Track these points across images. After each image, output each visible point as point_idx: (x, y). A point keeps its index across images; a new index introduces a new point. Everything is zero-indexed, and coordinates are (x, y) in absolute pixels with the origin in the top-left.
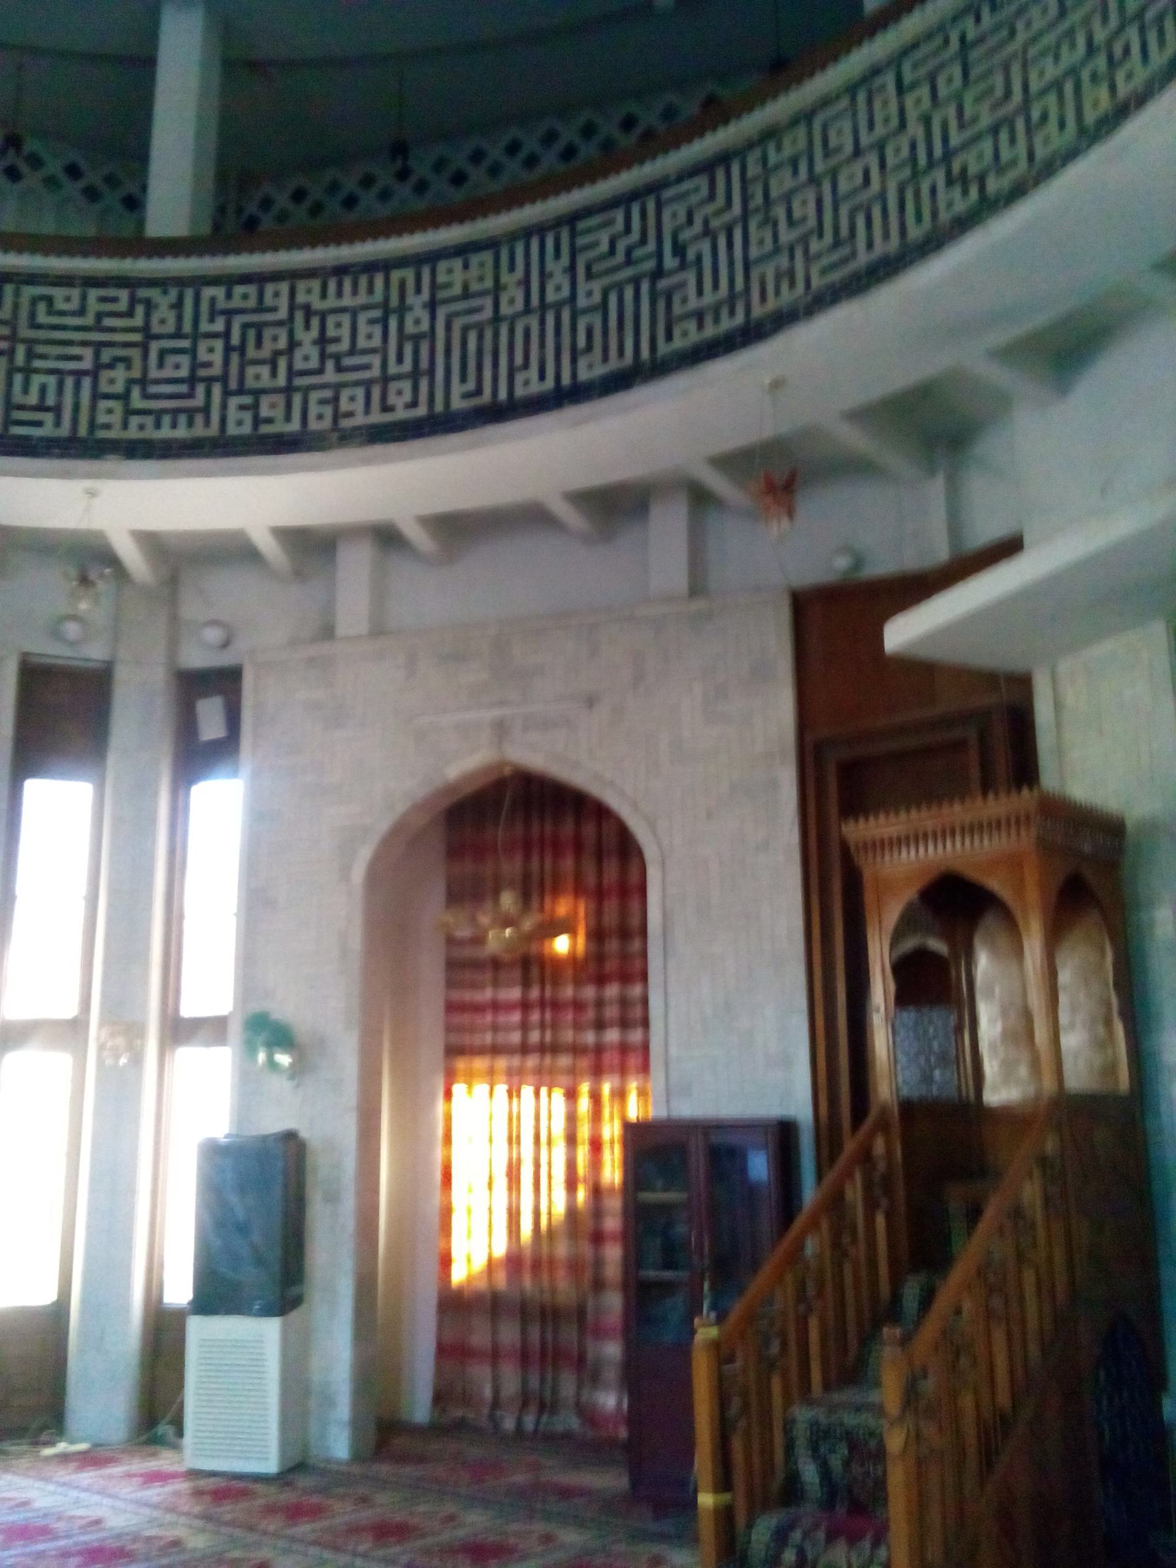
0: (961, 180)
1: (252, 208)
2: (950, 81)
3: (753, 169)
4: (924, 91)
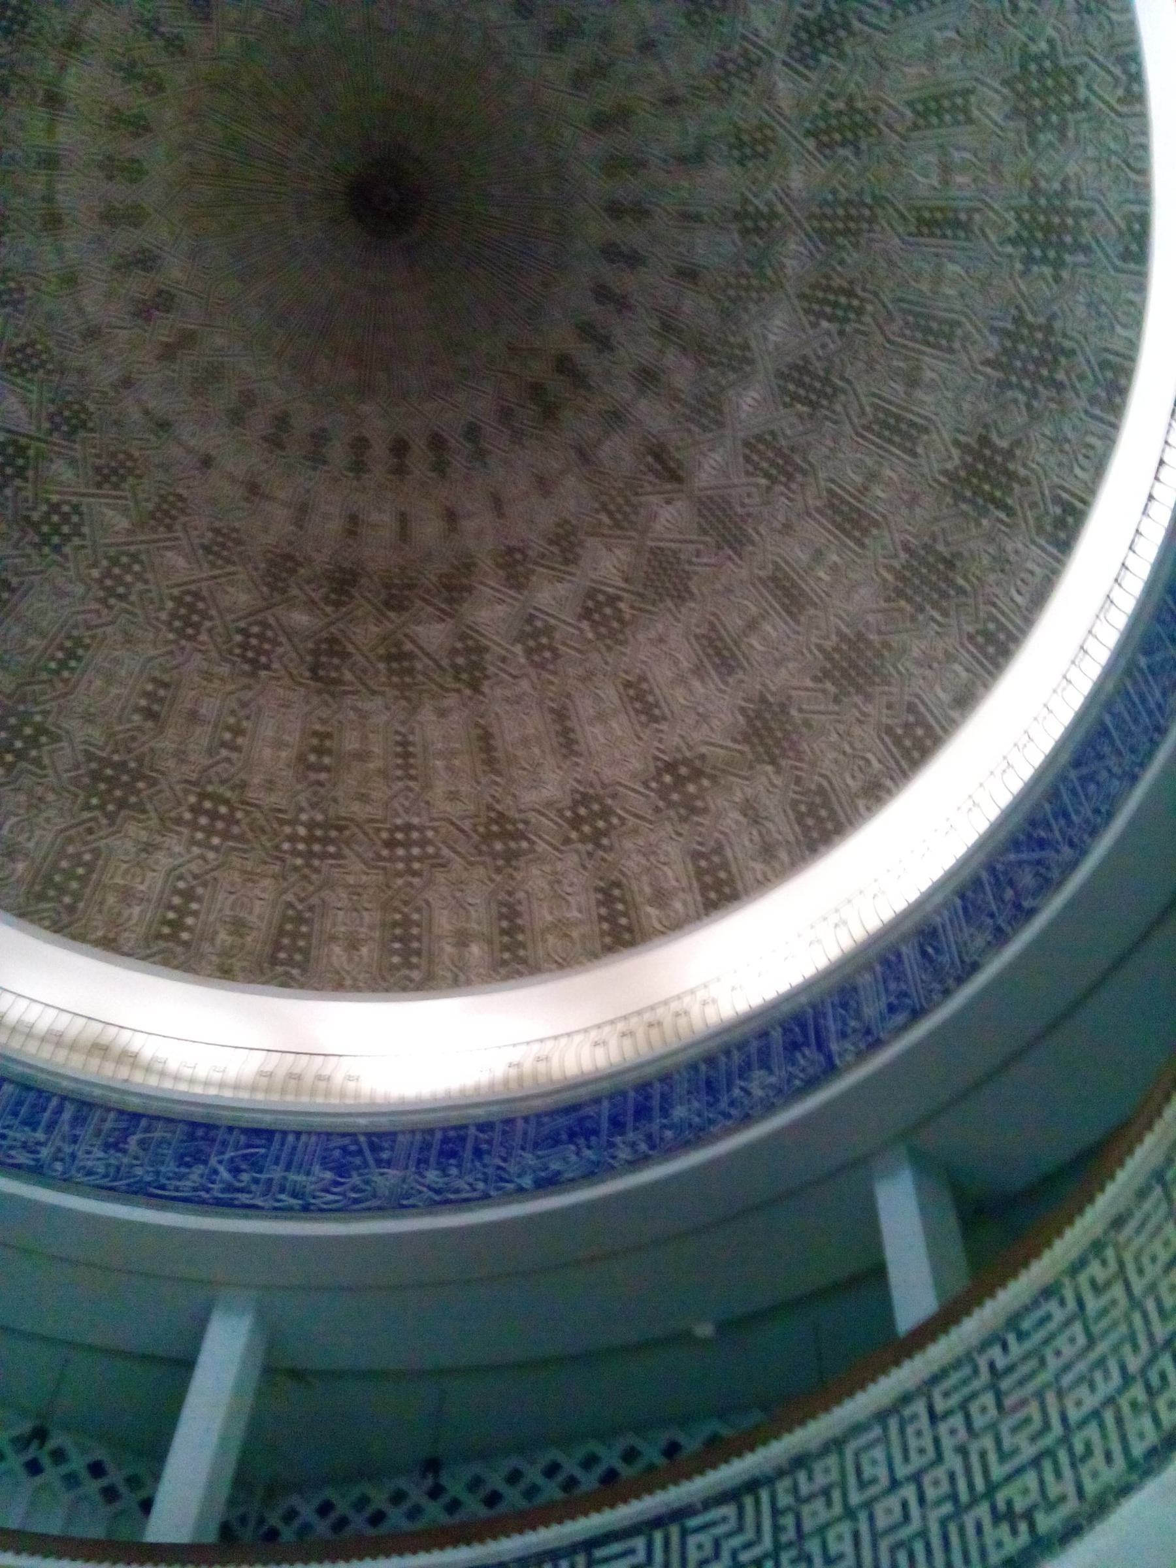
0: (1006, 1516)
1: (274, 1520)
2: (984, 1408)
3: (784, 1500)
4: (957, 1421)
